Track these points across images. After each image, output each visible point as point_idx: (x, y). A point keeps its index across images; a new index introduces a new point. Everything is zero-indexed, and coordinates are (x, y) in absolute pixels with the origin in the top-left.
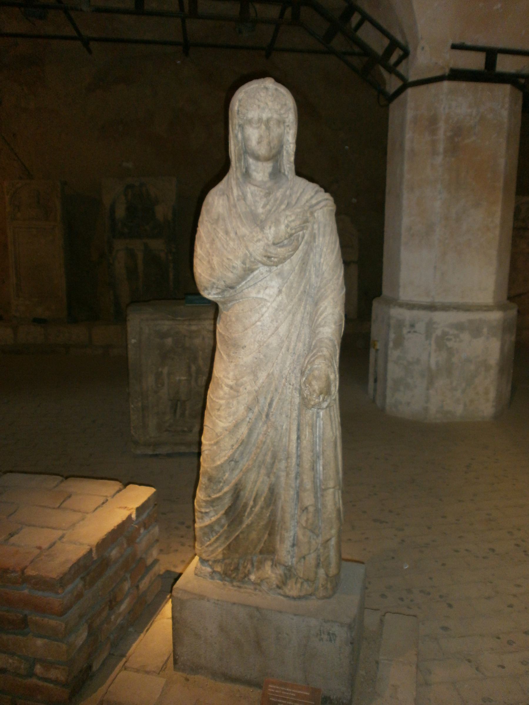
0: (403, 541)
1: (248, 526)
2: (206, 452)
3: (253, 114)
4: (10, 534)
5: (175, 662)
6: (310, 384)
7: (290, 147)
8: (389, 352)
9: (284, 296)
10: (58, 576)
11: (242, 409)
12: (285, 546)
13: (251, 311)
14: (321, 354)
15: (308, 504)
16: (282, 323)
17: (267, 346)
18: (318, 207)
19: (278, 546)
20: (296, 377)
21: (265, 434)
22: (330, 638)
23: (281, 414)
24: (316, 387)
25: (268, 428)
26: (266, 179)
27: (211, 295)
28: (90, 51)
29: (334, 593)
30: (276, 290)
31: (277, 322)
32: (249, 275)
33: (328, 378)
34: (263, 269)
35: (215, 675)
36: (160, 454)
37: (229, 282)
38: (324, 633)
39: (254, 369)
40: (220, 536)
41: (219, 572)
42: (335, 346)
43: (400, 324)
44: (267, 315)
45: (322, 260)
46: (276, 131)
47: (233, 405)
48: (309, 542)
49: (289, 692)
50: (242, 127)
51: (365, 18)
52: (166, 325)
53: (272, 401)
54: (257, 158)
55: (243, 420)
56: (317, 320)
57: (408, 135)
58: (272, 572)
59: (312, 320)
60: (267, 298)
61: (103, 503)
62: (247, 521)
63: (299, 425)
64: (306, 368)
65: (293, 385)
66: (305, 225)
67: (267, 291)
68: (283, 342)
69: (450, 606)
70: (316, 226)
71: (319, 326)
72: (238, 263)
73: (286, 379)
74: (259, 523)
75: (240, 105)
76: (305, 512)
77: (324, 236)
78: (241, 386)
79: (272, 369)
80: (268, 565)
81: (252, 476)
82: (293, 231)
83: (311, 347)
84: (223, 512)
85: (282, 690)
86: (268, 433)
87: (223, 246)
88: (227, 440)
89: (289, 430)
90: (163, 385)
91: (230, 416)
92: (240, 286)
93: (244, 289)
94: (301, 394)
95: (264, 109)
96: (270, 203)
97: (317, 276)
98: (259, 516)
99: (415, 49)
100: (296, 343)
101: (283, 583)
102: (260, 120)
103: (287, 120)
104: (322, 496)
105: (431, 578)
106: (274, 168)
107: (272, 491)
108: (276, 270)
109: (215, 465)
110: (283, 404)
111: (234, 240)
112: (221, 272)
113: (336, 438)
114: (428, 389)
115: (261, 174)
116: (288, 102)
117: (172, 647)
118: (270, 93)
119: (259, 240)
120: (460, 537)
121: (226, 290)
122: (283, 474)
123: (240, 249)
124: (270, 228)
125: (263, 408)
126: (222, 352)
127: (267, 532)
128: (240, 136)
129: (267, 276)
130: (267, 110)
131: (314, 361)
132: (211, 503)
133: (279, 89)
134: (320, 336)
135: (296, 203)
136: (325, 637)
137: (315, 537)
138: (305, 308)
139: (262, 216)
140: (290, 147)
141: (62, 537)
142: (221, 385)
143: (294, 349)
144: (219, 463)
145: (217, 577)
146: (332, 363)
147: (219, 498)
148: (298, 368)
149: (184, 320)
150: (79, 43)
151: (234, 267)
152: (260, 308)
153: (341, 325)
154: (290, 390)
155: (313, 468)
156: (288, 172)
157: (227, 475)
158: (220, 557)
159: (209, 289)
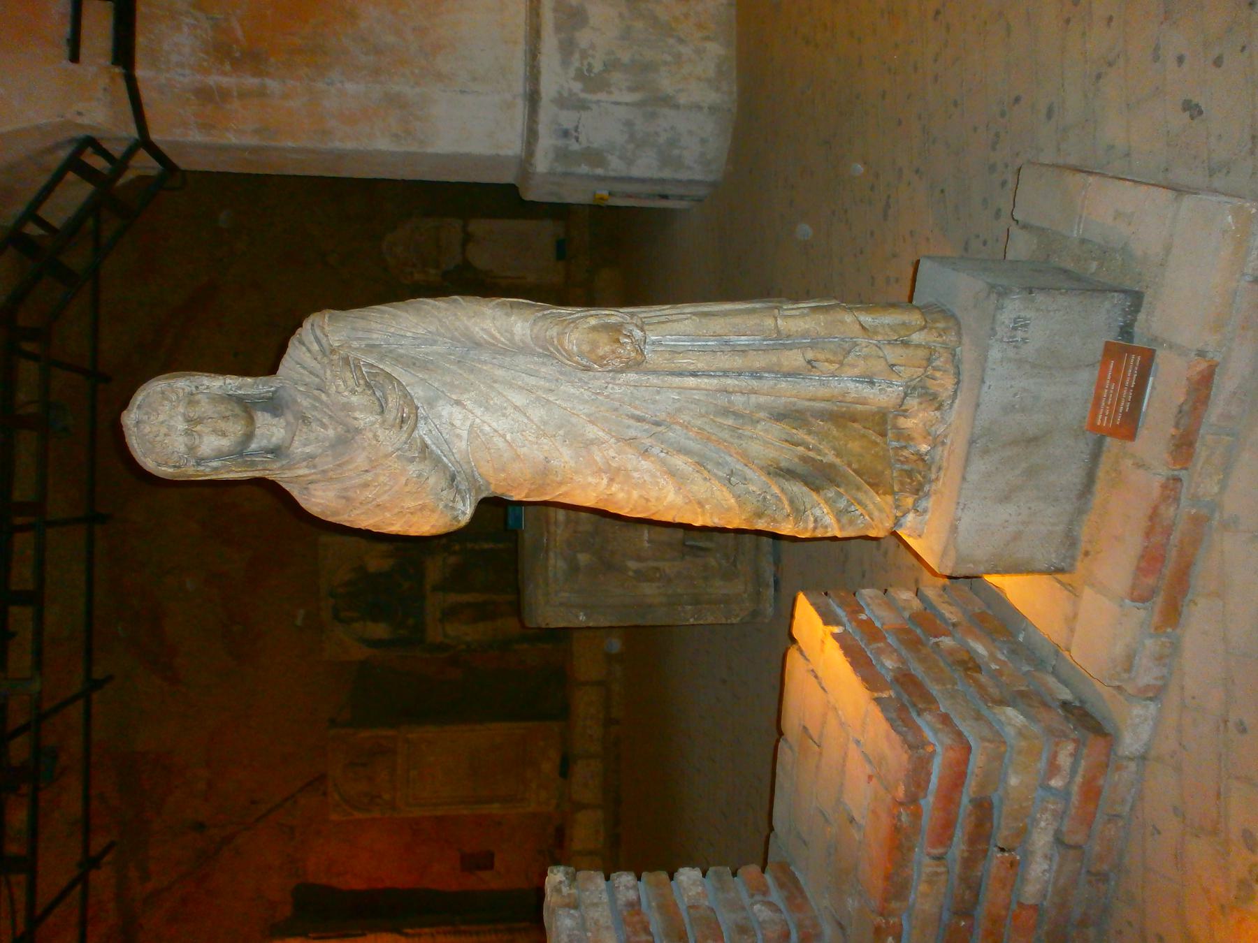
0: (917, 171)
1: (838, 455)
2: (716, 520)
3: (179, 444)
4: (851, 822)
5: (1060, 570)
6: (603, 358)
7: (232, 384)
8: (612, 174)
9: (466, 396)
10: (906, 752)
11: (645, 464)
12: (871, 396)
13: (489, 449)
14: (555, 340)
15: (802, 359)
16: (509, 400)
17: (545, 423)
18: (324, 341)
19: (874, 409)
20: (595, 378)
21: (687, 427)
22: (1021, 326)
23: (655, 402)
24: (607, 348)
25: (677, 423)
26: (282, 421)
27: (465, 511)
28: (110, 678)
29: (953, 316)
30: (456, 410)
31: (505, 408)
32: (432, 452)
33: (594, 329)
34: (422, 429)
35: (1081, 511)
36: (775, 576)
37: (444, 484)
38: (1014, 337)
39: (582, 445)
40: (856, 499)
41: (915, 500)
42: (544, 315)
43: (562, 155)
44: (494, 425)
45: (409, 334)
46: (205, 408)
47: (639, 478)
48: (866, 358)
49: (1108, 393)
50: (200, 461)
51: (31, 214)
52: (556, 564)
53: (633, 417)
54: (249, 436)
55: (663, 462)
56: (503, 343)
57: (232, 139)
58: (915, 417)
59: (504, 352)
60: (468, 423)
61: (816, 677)
62: (830, 457)
63: (673, 373)
64: (577, 363)
65: (608, 383)
66: (351, 363)
67: (457, 423)
68: (538, 399)
69: (1017, 100)
70: (355, 344)
71: (511, 340)
72: (412, 469)
73: (598, 394)
74: (834, 437)
75: (166, 464)
76: (814, 363)
77: (369, 331)
78: (610, 465)
79: (582, 416)
80: (907, 423)
81: (755, 448)
82: (362, 382)
83: (546, 354)
84: (814, 496)
85: (1106, 404)
86: (686, 423)
87: (386, 492)
88: (695, 488)
89: (682, 389)
90: (657, 569)
91: (657, 483)
92: (450, 465)
93: (455, 458)
94: (622, 371)
95: (170, 428)
96: (319, 416)
97: (434, 342)
98: (823, 436)
99: (82, 126)
100: (541, 378)
101: (931, 399)
102: (188, 433)
103: (187, 389)
104: (788, 337)
105: (975, 129)
106: (264, 410)
107: (780, 416)
108: (424, 409)
109: (737, 508)
110: (637, 399)
111: (377, 475)
112: (427, 496)
113: (694, 314)
114: (677, 107)
115: (274, 429)
116: (159, 389)
117: (1037, 577)
118: (145, 417)
119: (376, 437)
120: (916, 69)
121: (457, 487)
122: (753, 399)
123: (390, 466)
124: (356, 419)
125: (645, 430)
126: (557, 493)
127: (850, 424)
128: (215, 464)
129: (434, 423)
130: (172, 423)
131: (565, 350)
132: (798, 512)
133: (138, 403)
134: (528, 340)
135: (317, 376)
136: (1020, 334)
137: (857, 348)
138: (485, 362)
139: (339, 430)
140: (230, 384)
141: (858, 742)
142: (608, 495)
143: (549, 381)
144: (733, 501)
145: (923, 504)
146: (571, 321)
147: (791, 502)
148: (580, 374)
149: (548, 532)
150: (96, 696)
151: (419, 476)
152: (485, 434)
153: (512, 305)
154: (616, 388)
155: (743, 352)
156: (272, 387)
157: (752, 488)
158: (889, 499)
159: (455, 513)
